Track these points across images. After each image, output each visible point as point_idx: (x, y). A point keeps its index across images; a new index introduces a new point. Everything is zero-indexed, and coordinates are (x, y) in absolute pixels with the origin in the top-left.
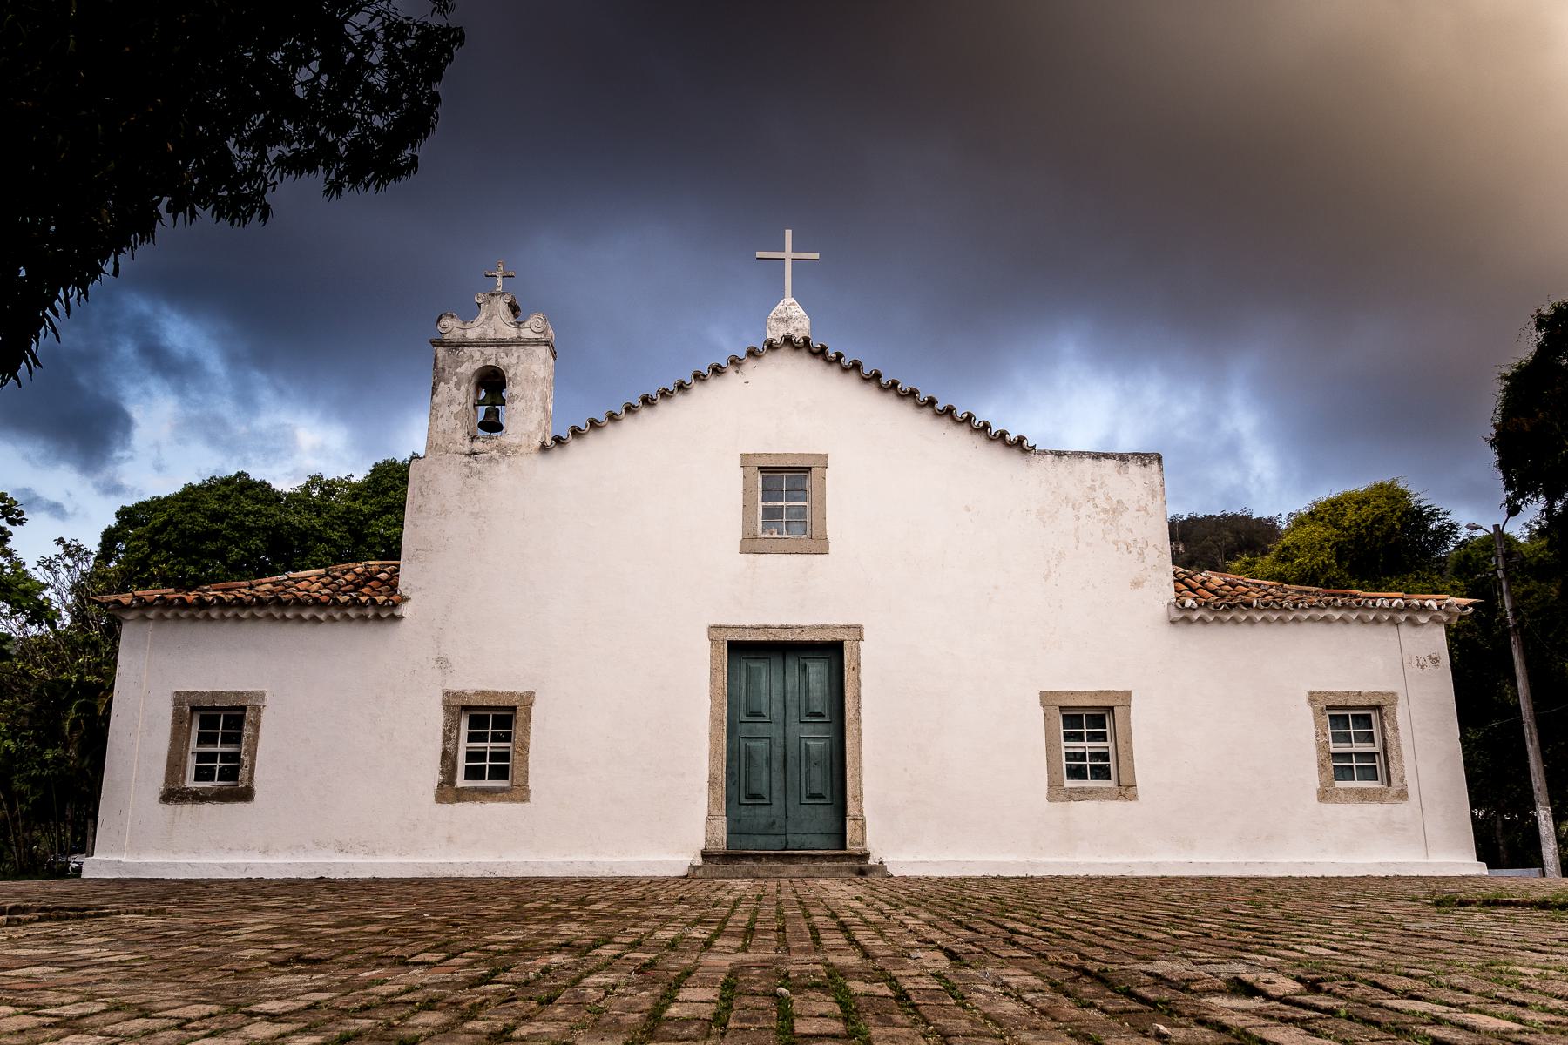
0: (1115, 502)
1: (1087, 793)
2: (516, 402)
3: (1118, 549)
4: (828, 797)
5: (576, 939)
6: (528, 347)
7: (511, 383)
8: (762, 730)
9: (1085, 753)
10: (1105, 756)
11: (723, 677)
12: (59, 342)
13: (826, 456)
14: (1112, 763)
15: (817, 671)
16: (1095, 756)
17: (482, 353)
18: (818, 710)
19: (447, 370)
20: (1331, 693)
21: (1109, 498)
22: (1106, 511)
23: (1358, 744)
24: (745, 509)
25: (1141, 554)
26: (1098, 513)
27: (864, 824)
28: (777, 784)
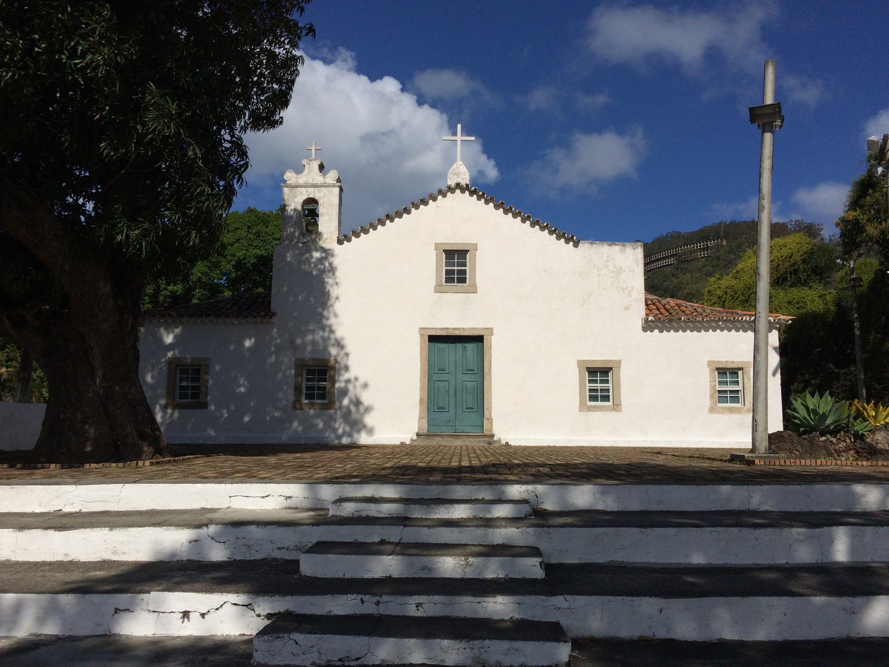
2: (324, 216)
3: (618, 291)
7: (321, 207)
11: (426, 353)
18: (471, 368)
22: (614, 272)
27: (492, 421)
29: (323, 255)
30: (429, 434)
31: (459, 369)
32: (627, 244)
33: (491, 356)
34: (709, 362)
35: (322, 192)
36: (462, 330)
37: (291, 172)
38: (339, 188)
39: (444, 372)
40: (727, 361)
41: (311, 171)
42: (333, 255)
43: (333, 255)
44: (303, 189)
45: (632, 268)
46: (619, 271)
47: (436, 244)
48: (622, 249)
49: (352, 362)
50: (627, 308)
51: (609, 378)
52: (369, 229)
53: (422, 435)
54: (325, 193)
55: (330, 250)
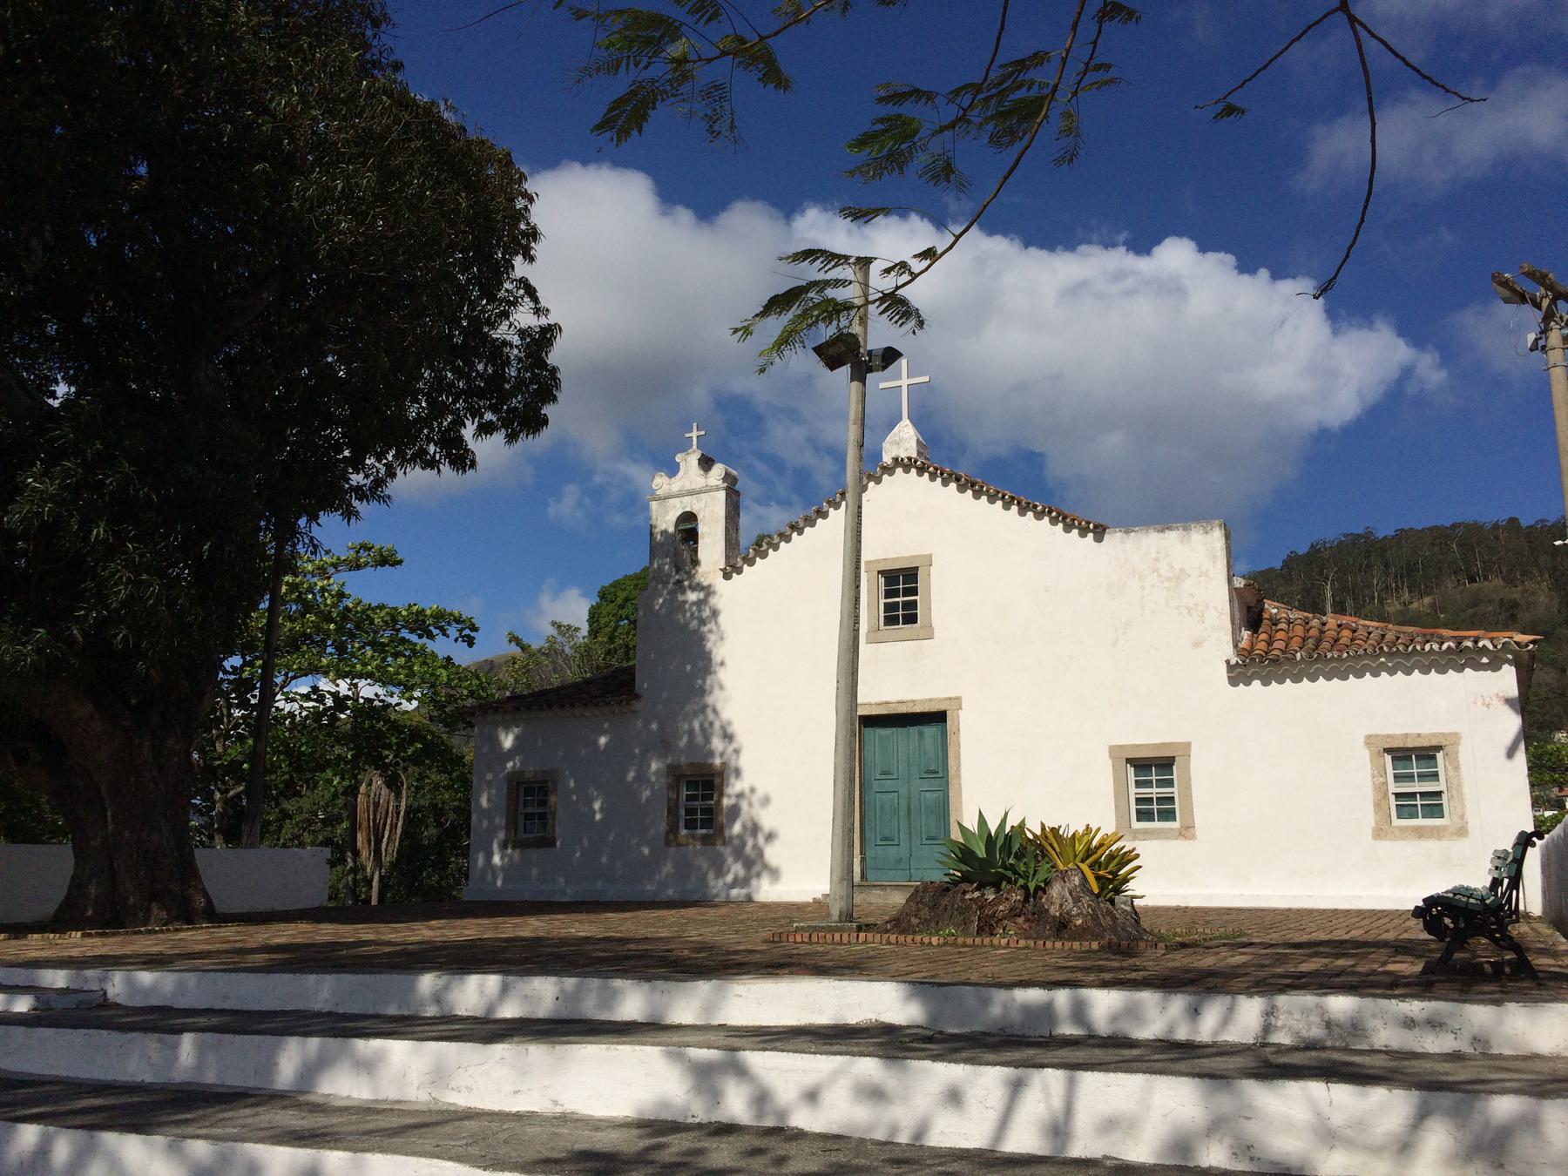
0: (1178, 570)
1: (1150, 833)
5: (1545, 952)
8: (889, 785)
13: (931, 556)
14: (1133, 807)
16: (1161, 800)
20: (1388, 736)
21: (1172, 568)
22: (1169, 579)
23: (1421, 784)
26: (1162, 582)
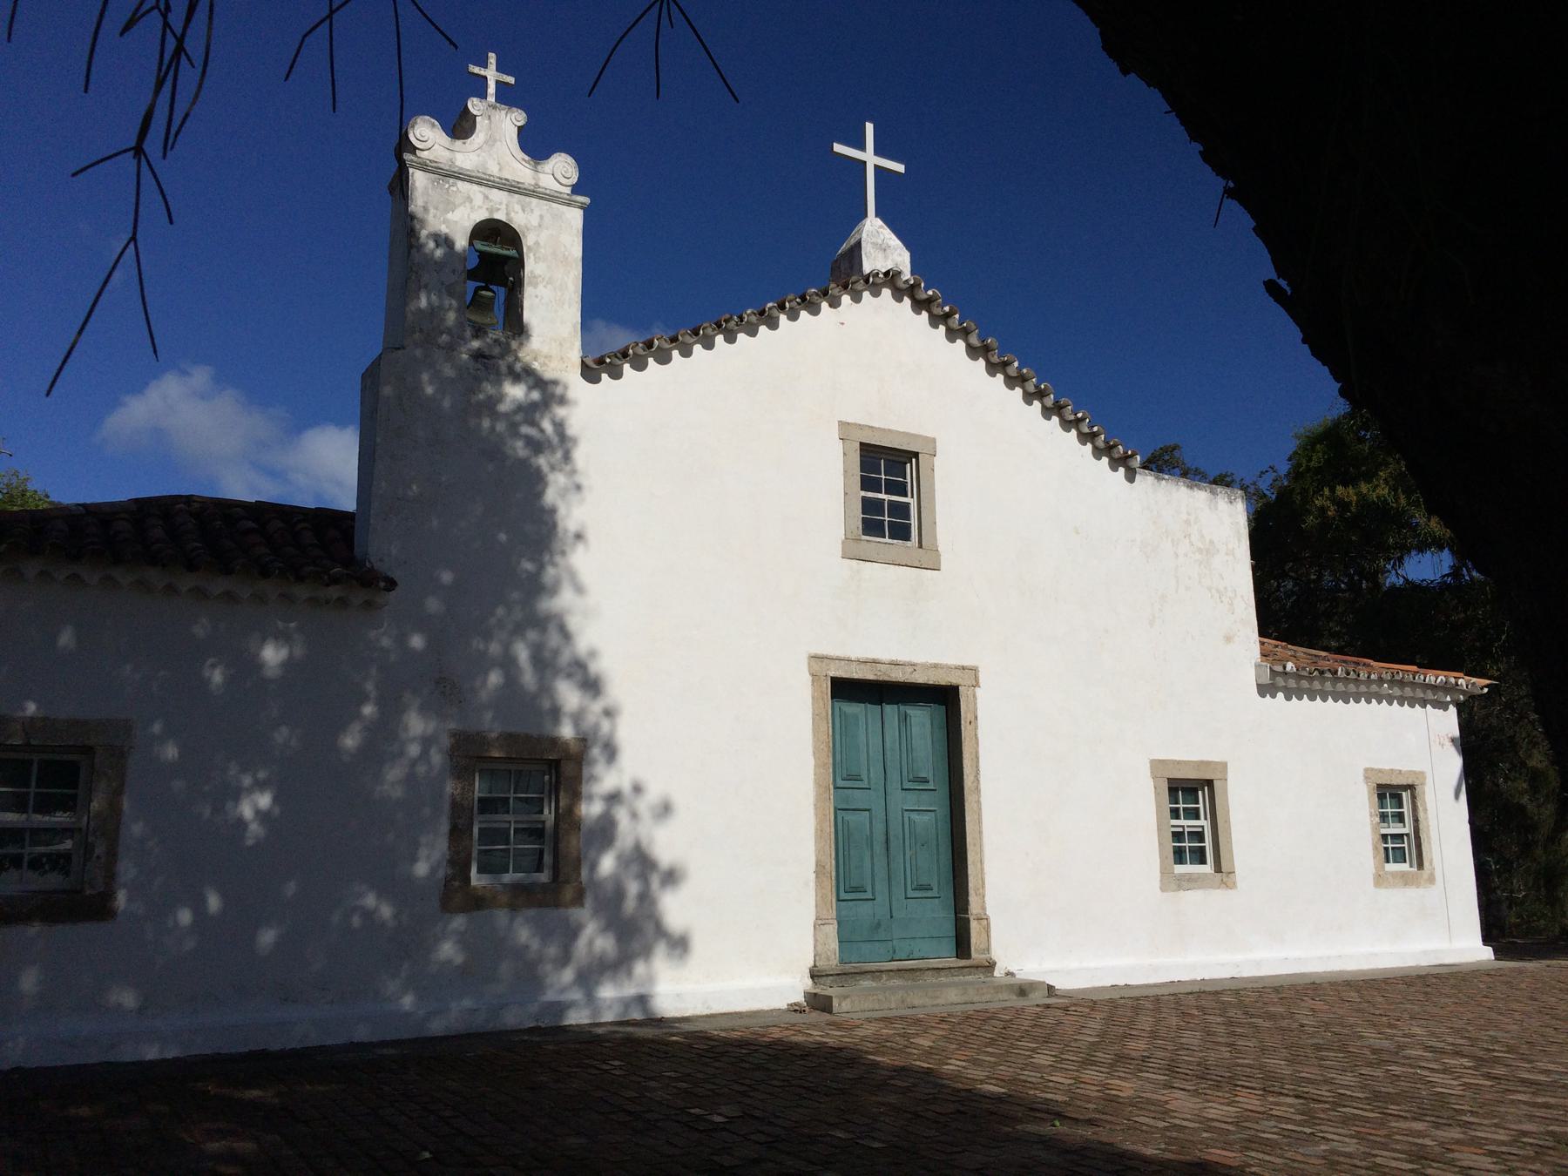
2: (541, 287)
3: (1212, 596)
4: (935, 889)
6: (554, 205)
7: (531, 255)
9: (1183, 832)
10: (1199, 836)
11: (826, 727)
12: (122, 34)
15: (922, 718)
17: (486, 197)
18: (923, 775)
19: (432, 211)
22: (1200, 550)
23: (1395, 825)
24: (847, 497)
25: (1232, 604)
27: (988, 924)
28: (881, 873)
29: (536, 395)
30: (848, 967)
31: (894, 776)
32: (1219, 490)
33: (977, 744)
34: (1366, 770)
35: (532, 211)
36: (909, 669)
37: (433, 125)
38: (581, 212)
39: (857, 784)
40: (1392, 770)
41: (495, 141)
42: (562, 401)
43: (562, 401)
44: (475, 187)
45: (1230, 547)
46: (1209, 551)
47: (842, 424)
48: (1211, 500)
49: (626, 733)
50: (1228, 639)
51: (1201, 805)
52: (670, 350)
53: (827, 975)
54: (541, 217)
55: (555, 383)
